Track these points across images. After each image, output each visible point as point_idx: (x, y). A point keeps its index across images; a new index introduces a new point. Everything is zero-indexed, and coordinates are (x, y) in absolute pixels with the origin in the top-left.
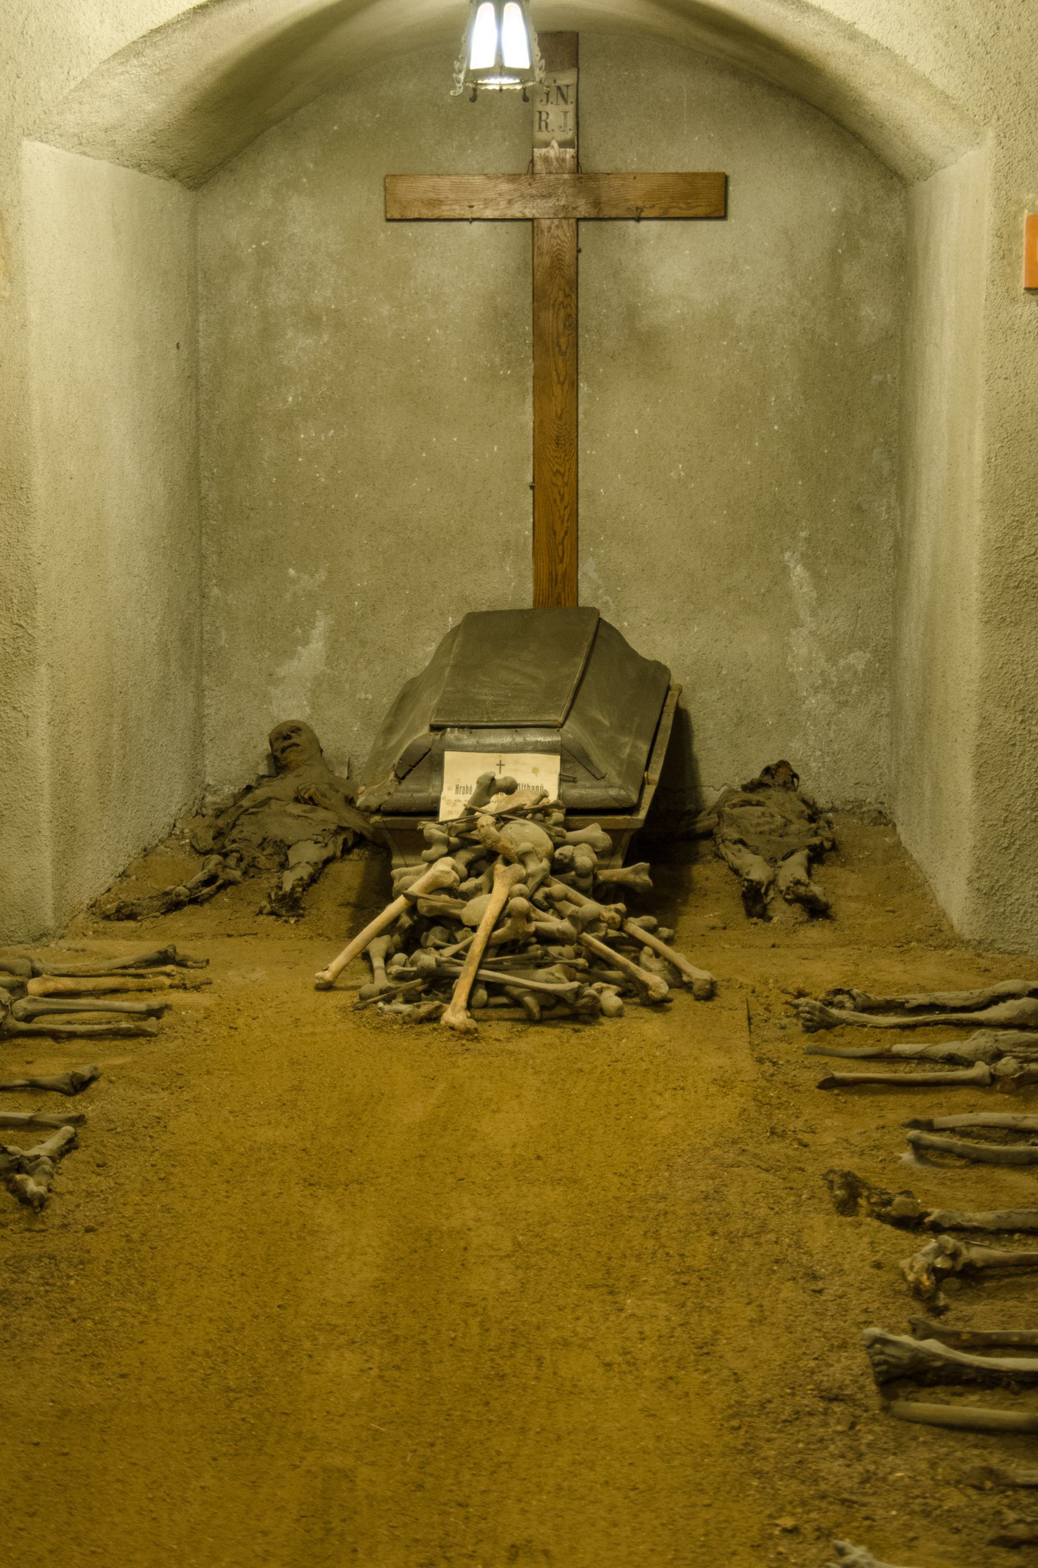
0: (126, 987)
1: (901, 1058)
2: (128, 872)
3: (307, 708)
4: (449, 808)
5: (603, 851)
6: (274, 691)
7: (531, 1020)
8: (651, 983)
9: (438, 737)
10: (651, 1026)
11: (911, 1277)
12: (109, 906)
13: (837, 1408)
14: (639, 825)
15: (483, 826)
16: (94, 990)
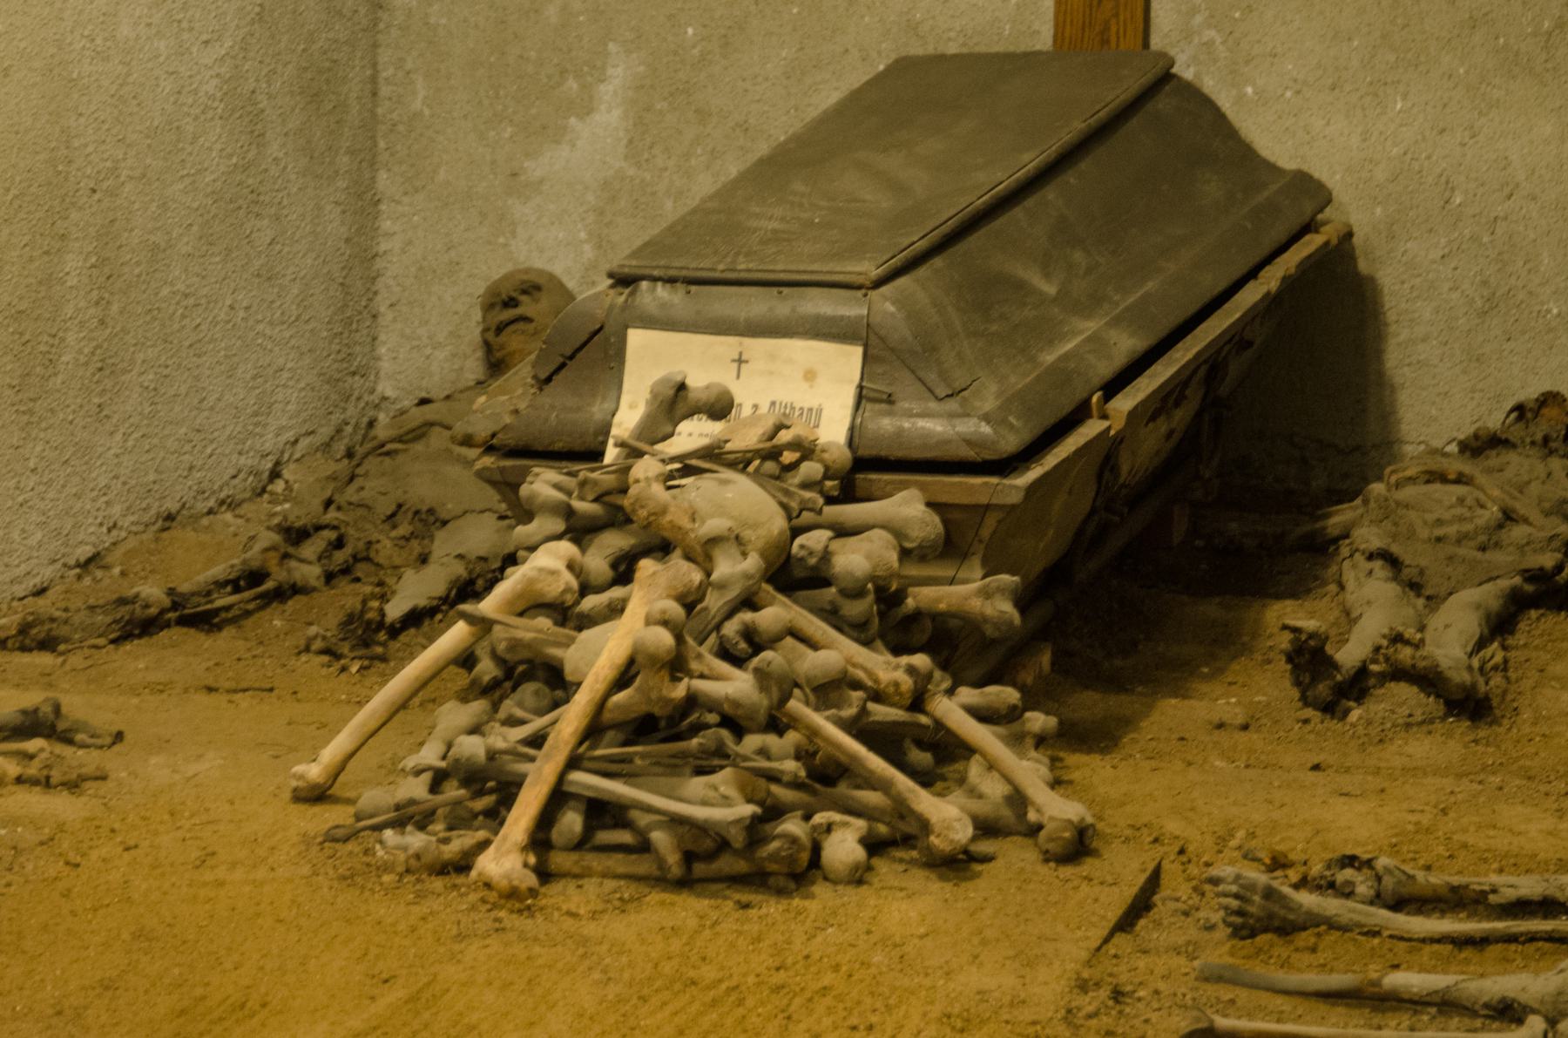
1: (1401, 1000)
2: (109, 560)
3: (587, 247)
5: (920, 547)
7: (661, 881)
8: (934, 820)
9: (622, 299)
10: (907, 904)
14: (1015, 498)
15: (637, 481)
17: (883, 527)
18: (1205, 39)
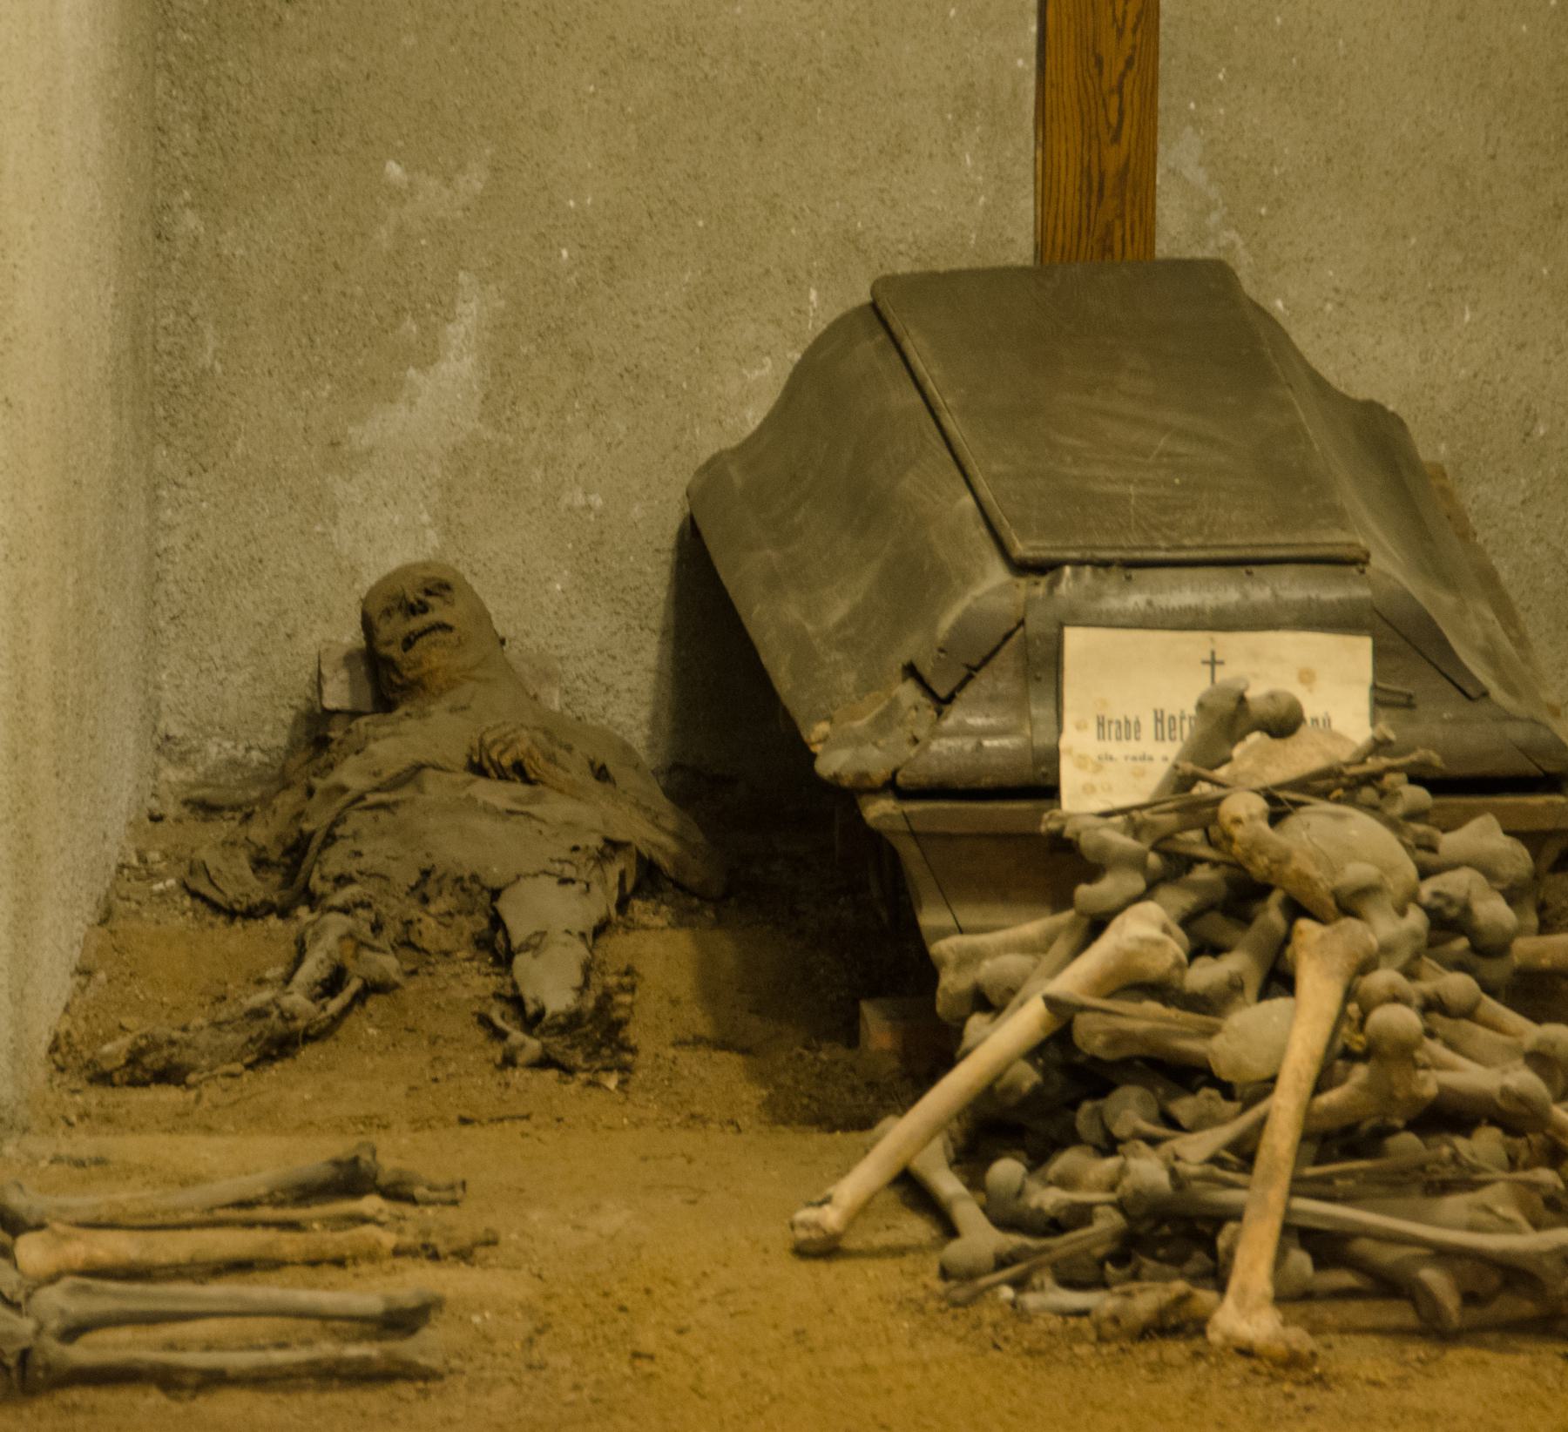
0: (276, 1254)
3: (430, 533)
4: (1083, 777)
6: (342, 488)
7: (1435, 1330)
12: (107, 1048)
15: (1237, 821)
16: (193, 1263)
17: (1468, 865)
18: (1223, 243)
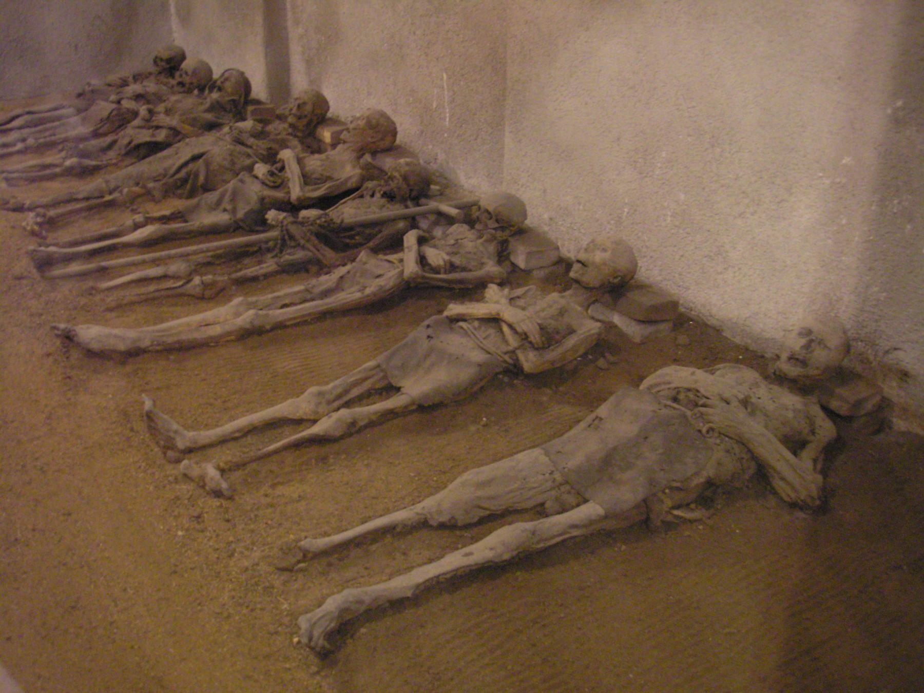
11: (29, 228)
13: (24, 282)
